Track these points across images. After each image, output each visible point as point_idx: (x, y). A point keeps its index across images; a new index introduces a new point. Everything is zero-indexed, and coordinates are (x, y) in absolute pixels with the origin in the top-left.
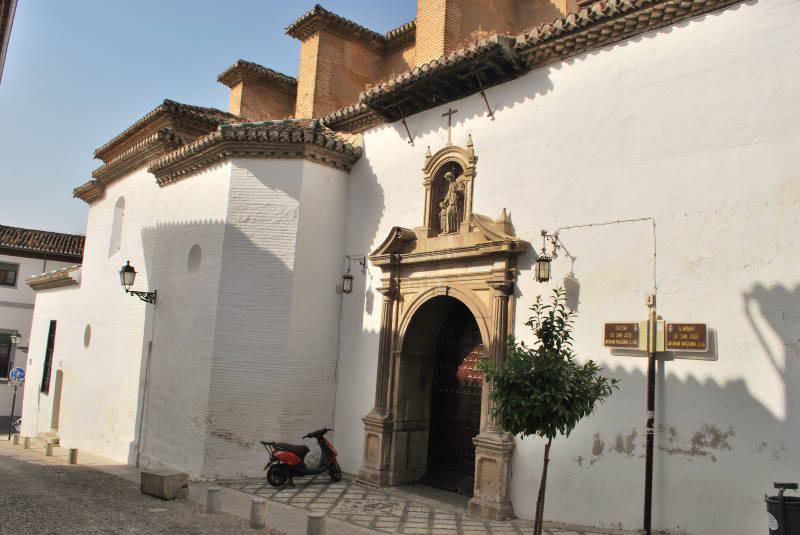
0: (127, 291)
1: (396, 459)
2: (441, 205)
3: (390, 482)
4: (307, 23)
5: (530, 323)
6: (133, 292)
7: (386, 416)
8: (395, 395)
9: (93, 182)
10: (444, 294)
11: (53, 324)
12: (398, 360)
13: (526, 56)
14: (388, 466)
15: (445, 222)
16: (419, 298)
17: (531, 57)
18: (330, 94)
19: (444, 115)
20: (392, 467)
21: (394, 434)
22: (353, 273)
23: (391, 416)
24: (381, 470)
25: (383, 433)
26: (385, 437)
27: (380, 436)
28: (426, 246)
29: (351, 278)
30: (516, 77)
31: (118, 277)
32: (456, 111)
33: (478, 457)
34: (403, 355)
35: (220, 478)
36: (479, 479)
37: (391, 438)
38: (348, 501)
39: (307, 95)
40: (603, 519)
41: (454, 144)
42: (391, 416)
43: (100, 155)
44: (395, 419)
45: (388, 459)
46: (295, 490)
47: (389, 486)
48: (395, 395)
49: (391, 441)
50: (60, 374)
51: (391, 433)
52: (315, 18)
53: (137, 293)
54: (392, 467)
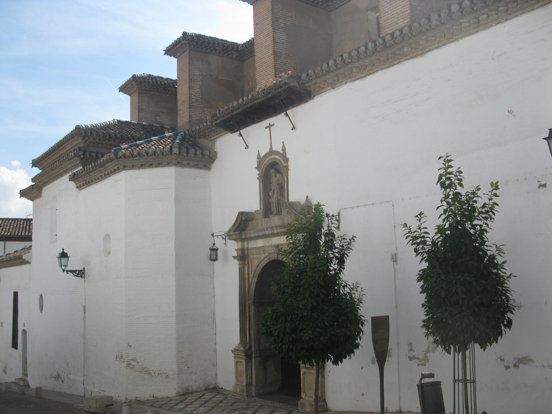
0: (64, 271)
1: (256, 376)
2: (270, 193)
3: (254, 394)
4: (178, 46)
5: (538, 182)
6: (67, 271)
7: (247, 348)
8: (252, 332)
9: (32, 185)
10: (276, 258)
11: (16, 294)
12: (252, 308)
13: (310, 86)
14: (251, 382)
15: (274, 208)
16: (261, 262)
17: (312, 87)
18: (202, 98)
19: (266, 128)
20: (254, 383)
21: (253, 360)
22: (218, 245)
23: (250, 347)
24: (247, 385)
25: (246, 360)
26: (247, 363)
27: (244, 361)
28: (262, 223)
29: (217, 250)
30: (307, 101)
31: (57, 260)
32: (273, 125)
33: (302, 372)
34: (255, 303)
35: (138, 399)
36: (304, 387)
37: (252, 363)
38: (219, 408)
39: (184, 102)
40: (374, 410)
41: (274, 149)
42: (250, 347)
43: (35, 163)
44: (253, 350)
45: (251, 377)
46: (214, 393)
47: (253, 397)
48: (252, 332)
49: (252, 365)
50: (24, 331)
51: (251, 360)
52: (183, 42)
53: (71, 271)
54: (254, 383)
